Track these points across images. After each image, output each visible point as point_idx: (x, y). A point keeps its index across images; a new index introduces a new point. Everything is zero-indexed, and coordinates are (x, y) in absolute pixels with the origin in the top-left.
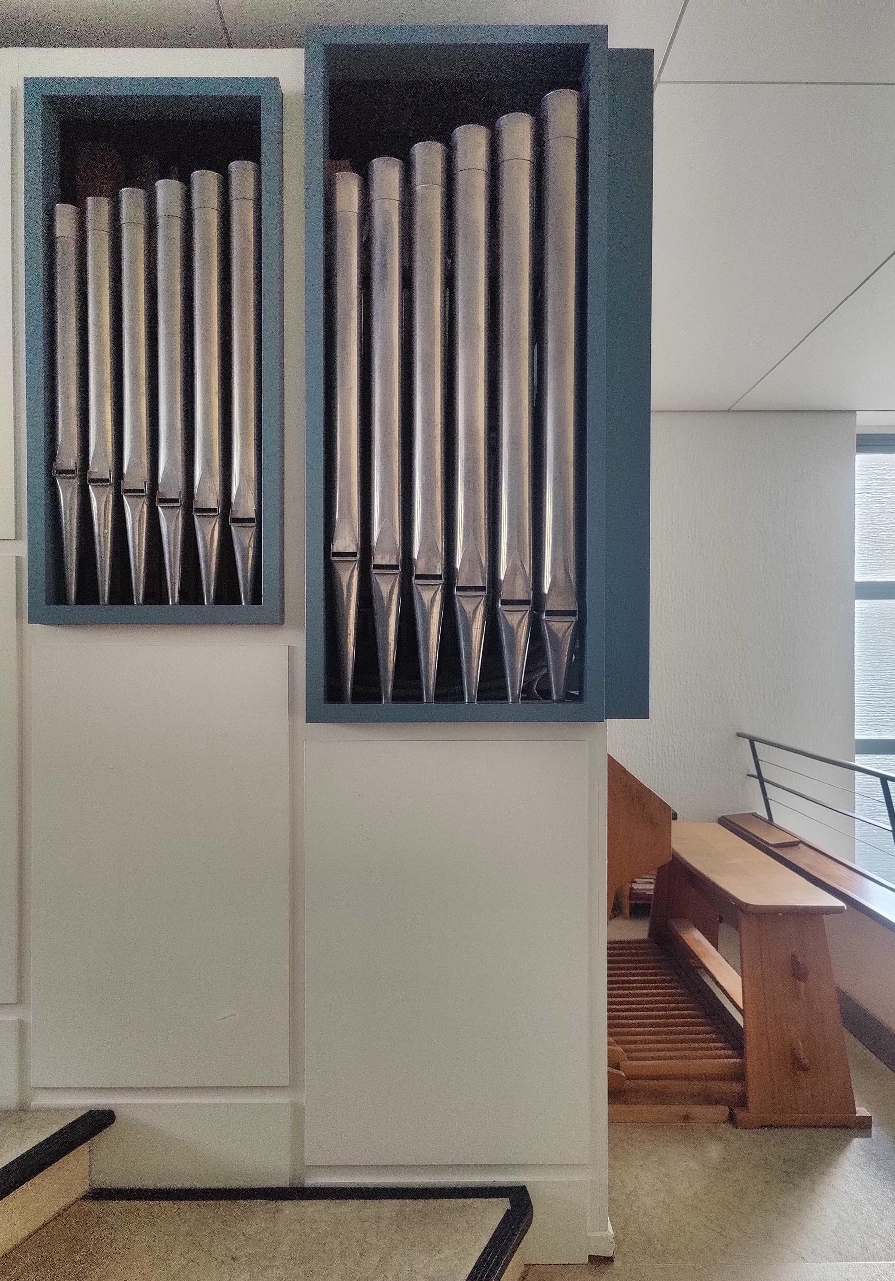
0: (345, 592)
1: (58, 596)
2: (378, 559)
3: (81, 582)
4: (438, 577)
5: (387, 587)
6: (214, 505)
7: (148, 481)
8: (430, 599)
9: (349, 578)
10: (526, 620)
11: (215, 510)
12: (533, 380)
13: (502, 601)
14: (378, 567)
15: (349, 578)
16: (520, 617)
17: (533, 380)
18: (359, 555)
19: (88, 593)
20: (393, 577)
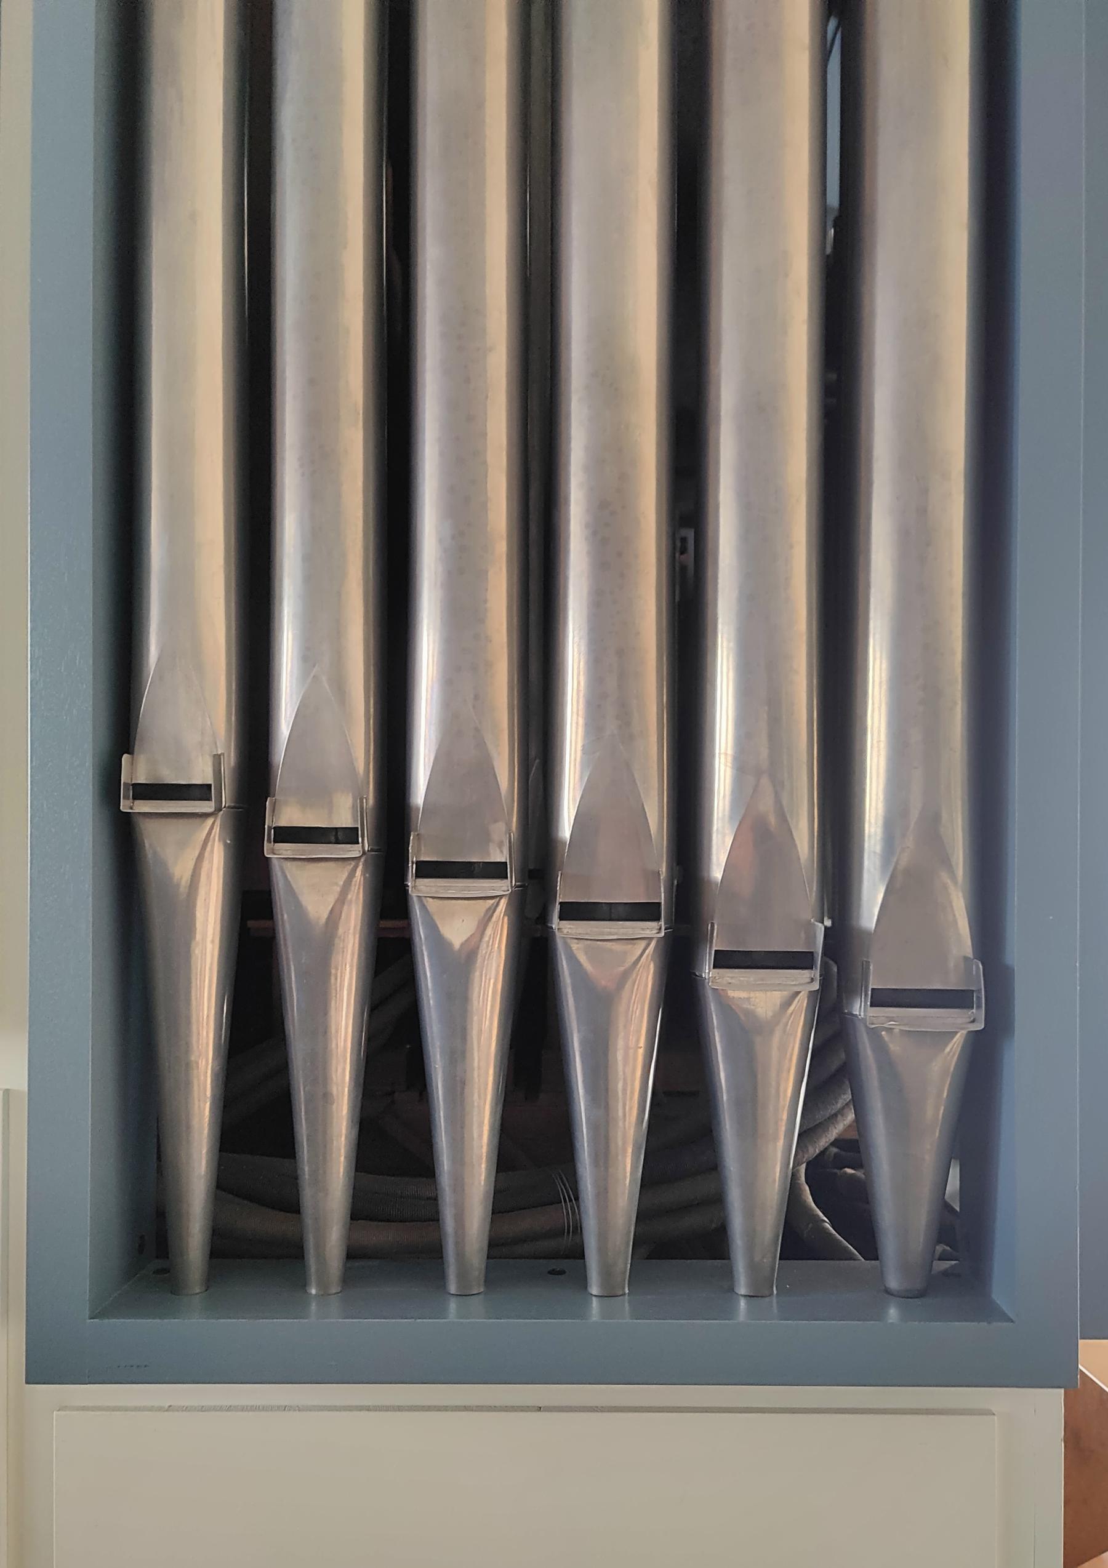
0: (774, 1083)
1: (145, 1253)
2: (288, 812)
3: (244, 1208)
4: (496, 871)
5: (325, 897)
6: (201, 773)
7: (230, 761)
8: (466, 930)
9: (195, 865)
10: (801, 1004)
11: (202, 792)
12: (382, 311)
13: (810, 967)
14: (288, 835)
15: (195, 865)
16: (345, 875)
17: (382, 311)
18: (365, 843)
20: (350, 866)
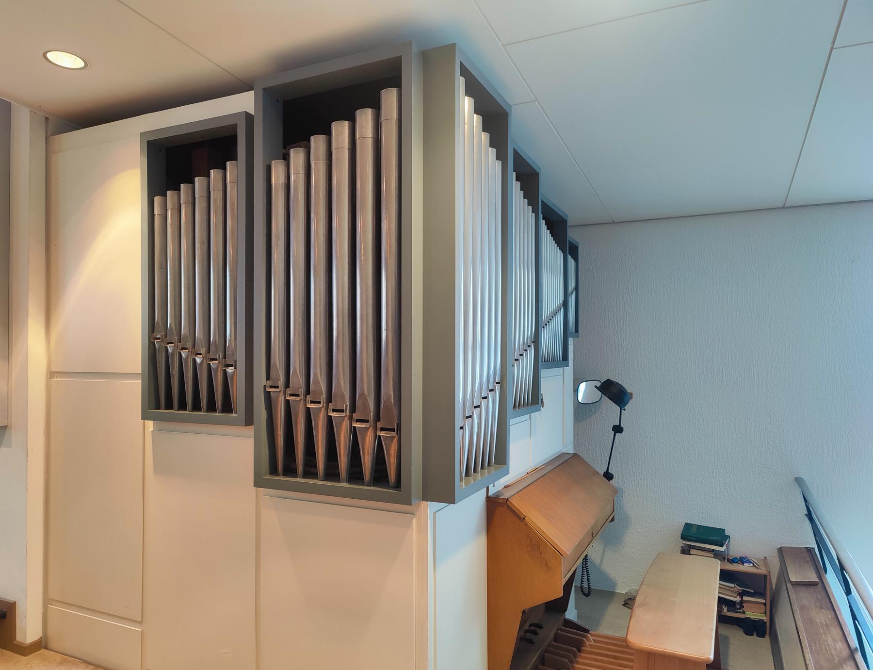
19: (290, 470)
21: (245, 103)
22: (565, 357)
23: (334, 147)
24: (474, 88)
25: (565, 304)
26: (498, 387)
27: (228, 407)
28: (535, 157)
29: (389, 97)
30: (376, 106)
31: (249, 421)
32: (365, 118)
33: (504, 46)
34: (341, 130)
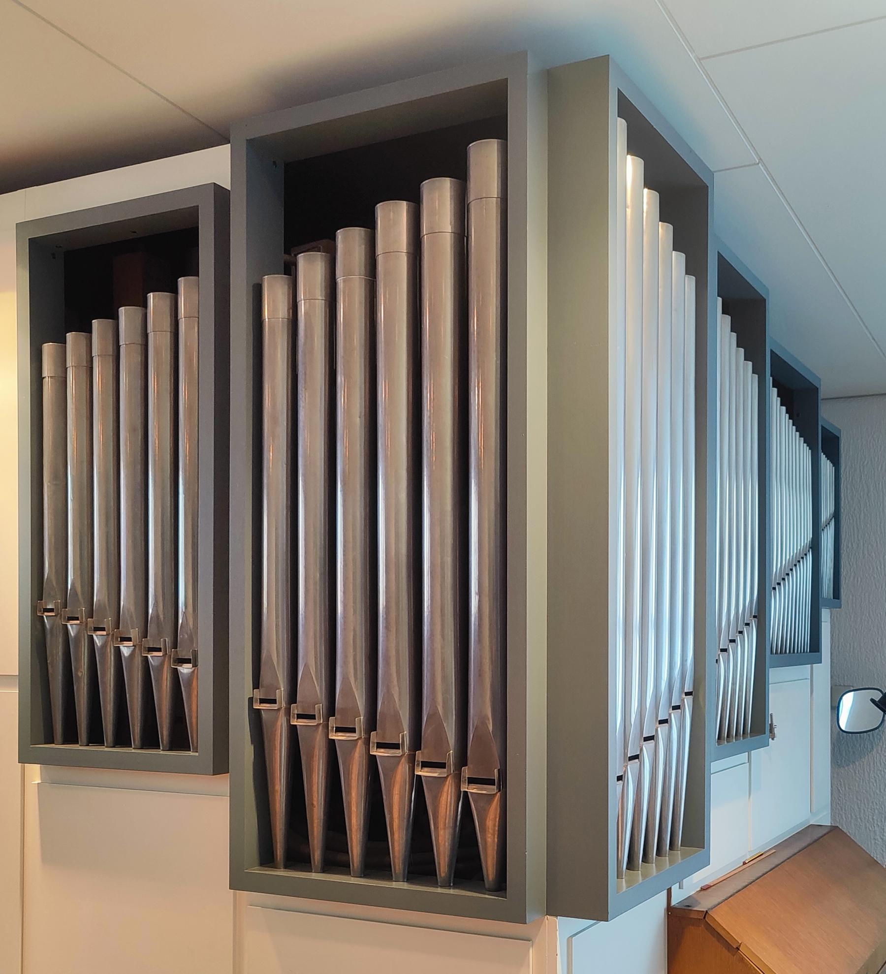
19: (297, 858)
21: (214, 166)
22: (815, 646)
23: (380, 250)
24: (645, 140)
25: (815, 546)
26: (688, 701)
27: (181, 739)
28: (759, 268)
29: (484, 156)
30: (460, 173)
31: (221, 765)
32: (439, 195)
33: (699, 60)
34: (393, 217)
